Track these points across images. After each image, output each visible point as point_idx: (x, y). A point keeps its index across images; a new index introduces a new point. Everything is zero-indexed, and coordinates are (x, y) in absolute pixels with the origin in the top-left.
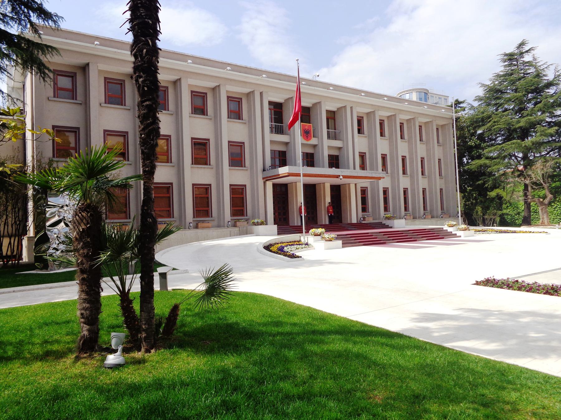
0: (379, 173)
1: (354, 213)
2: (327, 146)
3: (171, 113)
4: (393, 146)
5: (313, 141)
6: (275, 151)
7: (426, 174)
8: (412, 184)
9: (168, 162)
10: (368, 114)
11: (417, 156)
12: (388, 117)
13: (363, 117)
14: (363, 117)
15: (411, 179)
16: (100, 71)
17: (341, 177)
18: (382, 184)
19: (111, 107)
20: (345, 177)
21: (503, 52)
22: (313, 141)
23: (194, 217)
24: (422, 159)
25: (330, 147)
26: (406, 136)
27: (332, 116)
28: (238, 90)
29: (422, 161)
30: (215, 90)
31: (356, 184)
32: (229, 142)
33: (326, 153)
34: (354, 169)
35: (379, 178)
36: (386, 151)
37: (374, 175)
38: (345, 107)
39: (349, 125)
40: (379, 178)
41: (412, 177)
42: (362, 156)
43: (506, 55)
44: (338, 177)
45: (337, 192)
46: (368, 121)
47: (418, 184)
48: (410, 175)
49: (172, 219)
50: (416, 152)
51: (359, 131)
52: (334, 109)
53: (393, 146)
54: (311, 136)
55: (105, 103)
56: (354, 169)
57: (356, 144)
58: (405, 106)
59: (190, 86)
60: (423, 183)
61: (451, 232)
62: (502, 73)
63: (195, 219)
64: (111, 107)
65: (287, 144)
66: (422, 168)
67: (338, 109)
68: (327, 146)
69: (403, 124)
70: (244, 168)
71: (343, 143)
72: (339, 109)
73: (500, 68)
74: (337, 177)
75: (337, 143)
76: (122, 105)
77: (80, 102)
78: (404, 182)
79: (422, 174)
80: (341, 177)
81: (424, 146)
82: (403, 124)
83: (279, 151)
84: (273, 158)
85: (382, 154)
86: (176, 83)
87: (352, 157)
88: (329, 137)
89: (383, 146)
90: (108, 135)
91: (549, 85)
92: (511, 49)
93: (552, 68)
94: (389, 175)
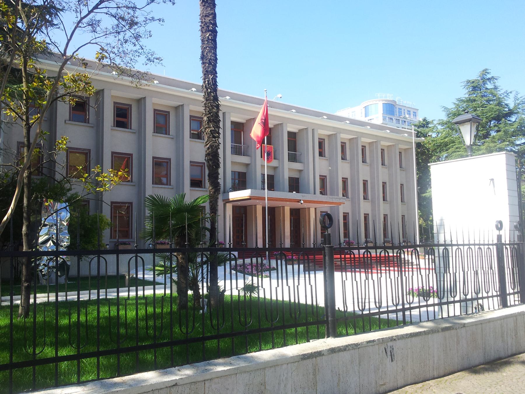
0: (340, 199)
1: (258, 235)
2: (287, 169)
3: (171, 137)
4: (354, 170)
5: (274, 163)
6: (235, 172)
7: (388, 199)
8: (373, 210)
9: (167, 185)
10: (329, 136)
11: (378, 181)
12: (350, 140)
13: (324, 140)
14: (324, 140)
15: (372, 205)
18: (342, 210)
19: (72, 124)
20: (305, 201)
21: (465, 79)
22: (274, 163)
23: (111, 238)
24: (384, 184)
25: (290, 170)
26: (368, 160)
27: (292, 136)
28: (163, 103)
29: (383, 186)
30: (178, 109)
31: (315, 209)
32: (191, 162)
33: (286, 176)
34: (315, 194)
35: (340, 204)
36: (347, 175)
37: (334, 201)
38: (306, 129)
39: (309, 148)
40: (340, 204)
41: (373, 202)
42: (323, 179)
43: (468, 82)
44: (299, 201)
45: (297, 215)
46: (329, 144)
47: (379, 210)
48: (352, 198)
49: (130, 240)
50: (378, 176)
51: (321, 154)
52: (243, 121)
53: (354, 170)
54: (272, 158)
55: (70, 120)
56: (315, 194)
57: (315, 167)
58: (367, 130)
59: (154, 104)
60: (383, 208)
62: (464, 99)
63: (112, 240)
64: (72, 124)
65: (247, 165)
66: (384, 193)
67: (299, 130)
68: (262, 166)
69: (365, 147)
70: (204, 189)
71: (251, 160)
72: (300, 130)
73: (463, 93)
74: (298, 202)
75: (297, 166)
76: (85, 122)
77: (92, 126)
78: (365, 207)
79: (384, 200)
80: (302, 202)
81: (386, 170)
82: (365, 147)
83: (239, 173)
84: (233, 179)
85: (343, 178)
86: (100, 93)
87: (312, 180)
88: (290, 160)
89: (364, 172)
90: (71, 152)
91: (511, 113)
92: (474, 76)
93: (512, 96)
94: (350, 199)
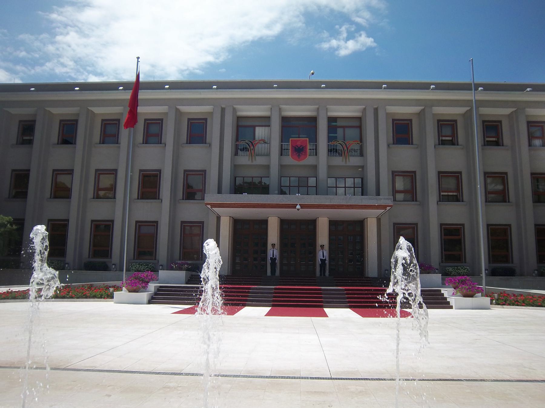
5: (309, 160)
16: (388, 114)
17: (298, 207)
56: (378, 194)
61: (446, 298)
